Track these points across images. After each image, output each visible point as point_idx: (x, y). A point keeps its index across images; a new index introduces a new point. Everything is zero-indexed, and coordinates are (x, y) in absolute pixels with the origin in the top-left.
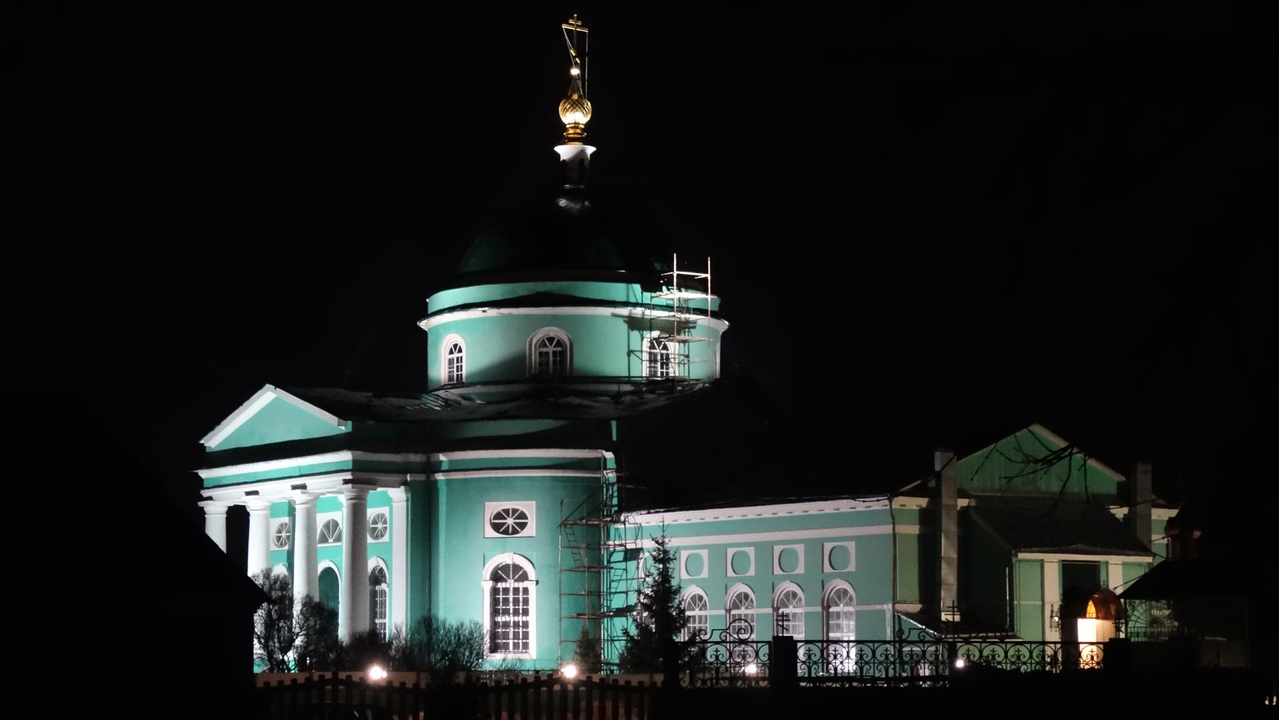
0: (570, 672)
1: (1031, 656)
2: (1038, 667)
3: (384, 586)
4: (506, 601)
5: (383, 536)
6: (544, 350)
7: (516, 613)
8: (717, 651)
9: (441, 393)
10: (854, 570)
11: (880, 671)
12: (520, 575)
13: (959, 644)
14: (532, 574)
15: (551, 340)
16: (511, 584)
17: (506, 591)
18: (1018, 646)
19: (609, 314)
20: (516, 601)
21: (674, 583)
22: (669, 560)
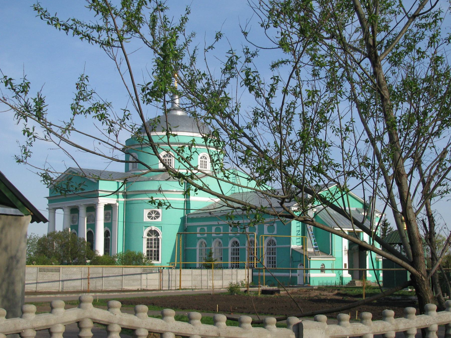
3: (109, 237)
4: (151, 243)
20: (155, 243)
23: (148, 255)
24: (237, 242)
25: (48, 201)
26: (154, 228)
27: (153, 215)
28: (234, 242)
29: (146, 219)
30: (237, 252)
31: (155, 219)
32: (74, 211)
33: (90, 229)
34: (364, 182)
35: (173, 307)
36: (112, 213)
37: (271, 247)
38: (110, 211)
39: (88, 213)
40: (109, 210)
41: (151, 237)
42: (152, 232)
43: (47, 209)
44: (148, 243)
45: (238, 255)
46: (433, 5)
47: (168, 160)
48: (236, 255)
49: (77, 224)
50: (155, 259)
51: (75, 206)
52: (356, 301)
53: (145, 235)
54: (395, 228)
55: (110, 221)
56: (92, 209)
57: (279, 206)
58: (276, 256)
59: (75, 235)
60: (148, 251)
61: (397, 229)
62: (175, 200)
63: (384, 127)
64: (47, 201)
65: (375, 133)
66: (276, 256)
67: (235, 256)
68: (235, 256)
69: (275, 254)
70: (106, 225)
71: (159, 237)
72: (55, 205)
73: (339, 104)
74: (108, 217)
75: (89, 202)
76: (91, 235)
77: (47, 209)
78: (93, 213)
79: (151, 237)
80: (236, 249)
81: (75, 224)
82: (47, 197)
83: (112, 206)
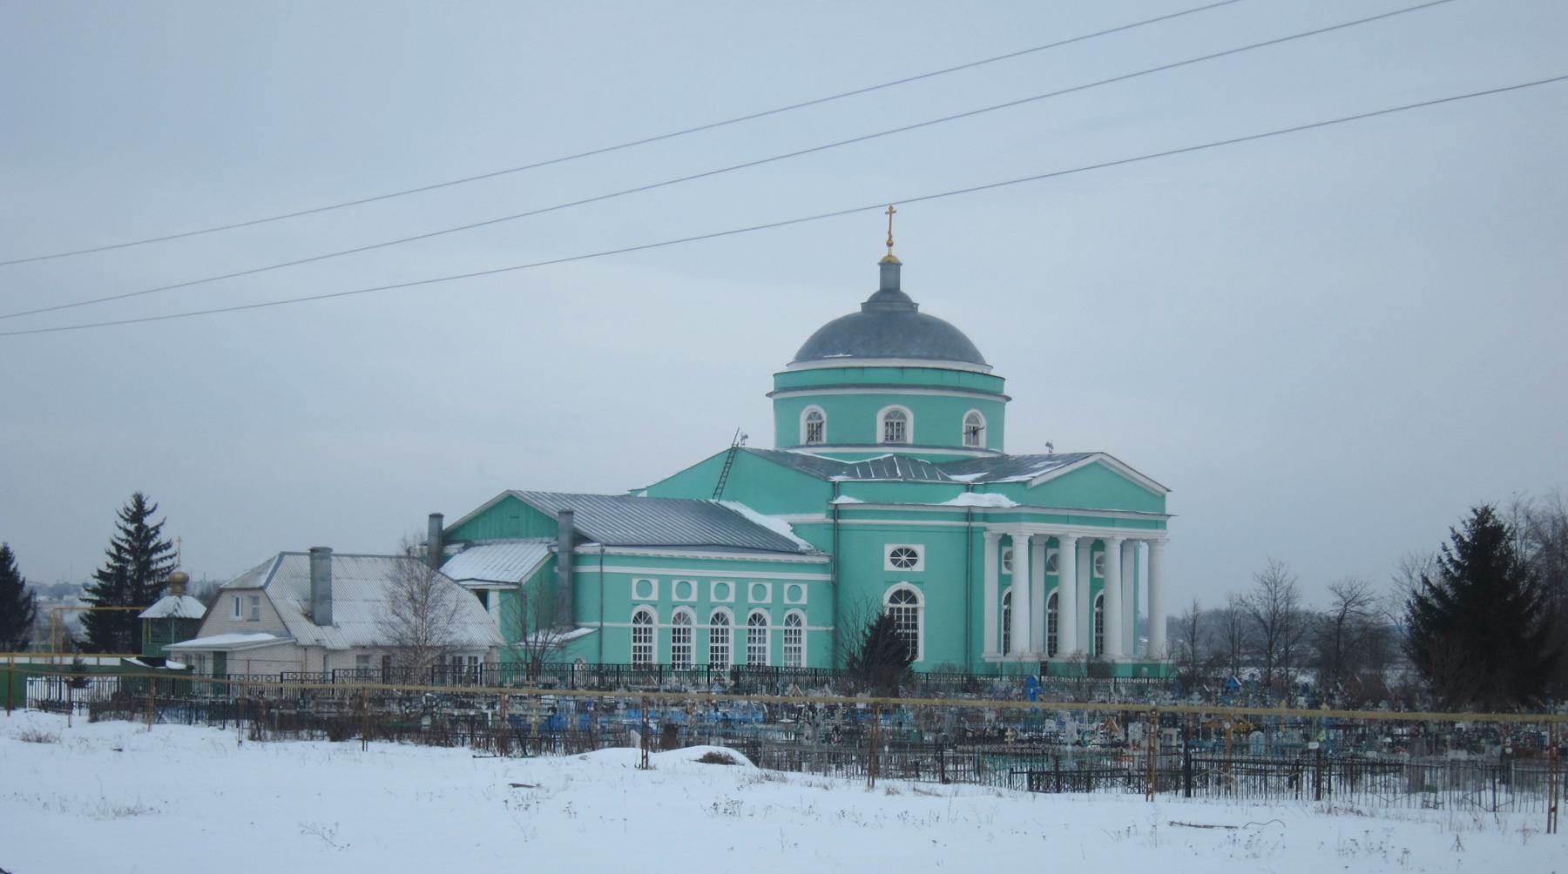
17: (899, 610)
20: (907, 618)
26: (904, 585)
27: (904, 558)
29: (889, 566)
30: (715, 636)
41: (898, 606)
44: (915, 618)
45: (712, 647)
48: (717, 648)
52: (728, 745)
58: (785, 645)
61: (1147, 617)
63: (1556, 815)
65: (1556, 803)
66: (785, 645)
67: (720, 645)
68: (720, 645)
69: (635, 647)
73: (893, 215)
74: (904, 558)
79: (898, 606)
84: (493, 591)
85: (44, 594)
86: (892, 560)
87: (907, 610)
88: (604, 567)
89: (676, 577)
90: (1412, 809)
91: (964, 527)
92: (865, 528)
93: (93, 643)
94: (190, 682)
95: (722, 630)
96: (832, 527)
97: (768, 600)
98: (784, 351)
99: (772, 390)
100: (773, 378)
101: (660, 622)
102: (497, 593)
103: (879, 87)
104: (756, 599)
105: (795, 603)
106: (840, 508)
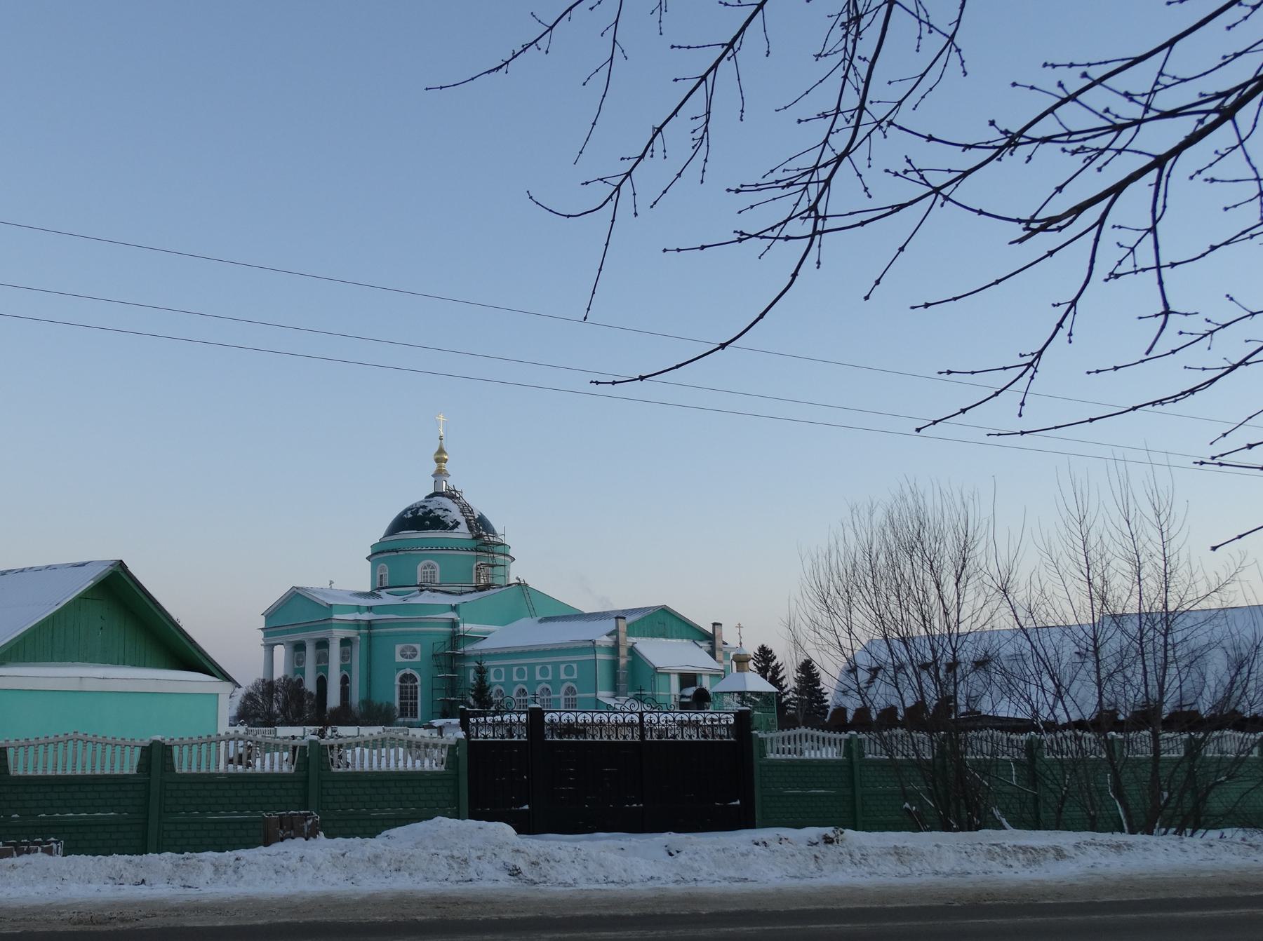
0: (969, 710)
1: (659, 722)
2: (581, 728)
3: (348, 685)
4: (406, 693)
5: (403, 657)
6: (425, 570)
7: (411, 698)
8: (616, 718)
9: (1250, 785)
10: (397, 661)
11: (597, 731)
12: (414, 679)
13: (644, 714)
14: (419, 679)
15: (429, 566)
16: (409, 684)
17: (407, 687)
18: (651, 714)
19: (627, 617)
20: (411, 693)
21: (487, 684)
22: (485, 672)
23: (402, 709)
24: (524, 690)
25: (263, 633)
26: (408, 671)
28: (519, 690)
29: (399, 659)
31: (411, 658)
32: (299, 647)
33: (321, 674)
34: (876, 124)
35: (616, 683)
36: (351, 651)
37: (570, 696)
38: (349, 648)
39: (343, 648)
40: (347, 646)
42: (405, 678)
43: (262, 645)
44: (401, 693)
46: (868, 137)
47: (431, 572)
48: (544, 700)
49: (303, 666)
50: (411, 715)
51: (300, 641)
53: (397, 682)
54: (912, 733)
55: (349, 662)
56: (323, 644)
57: (858, 669)
59: (300, 682)
60: (401, 704)
62: (406, 631)
64: (262, 633)
70: (342, 667)
71: (416, 683)
72: (272, 640)
75: (319, 634)
76: (322, 683)
77: (262, 645)
78: (325, 650)
80: (523, 700)
81: (346, 663)
82: (262, 629)
83: (352, 640)
84: (705, 675)
85: (297, 707)
86: (416, 651)
87: (411, 687)
88: (597, 655)
89: (538, 664)
90: (861, 857)
91: (374, 629)
92: (388, 635)
93: (874, 717)
94: (845, 739)
95: (547, 700)
96: (366, 635)
97: (550, 678)
98: (377, 530)
99: (370, 554)
100: (370, 549)
101: (559, 693)
102: (708, 677)
103: (851, 161)
104: (567, 675)
105: (545, 679)
106: (373, 623)
